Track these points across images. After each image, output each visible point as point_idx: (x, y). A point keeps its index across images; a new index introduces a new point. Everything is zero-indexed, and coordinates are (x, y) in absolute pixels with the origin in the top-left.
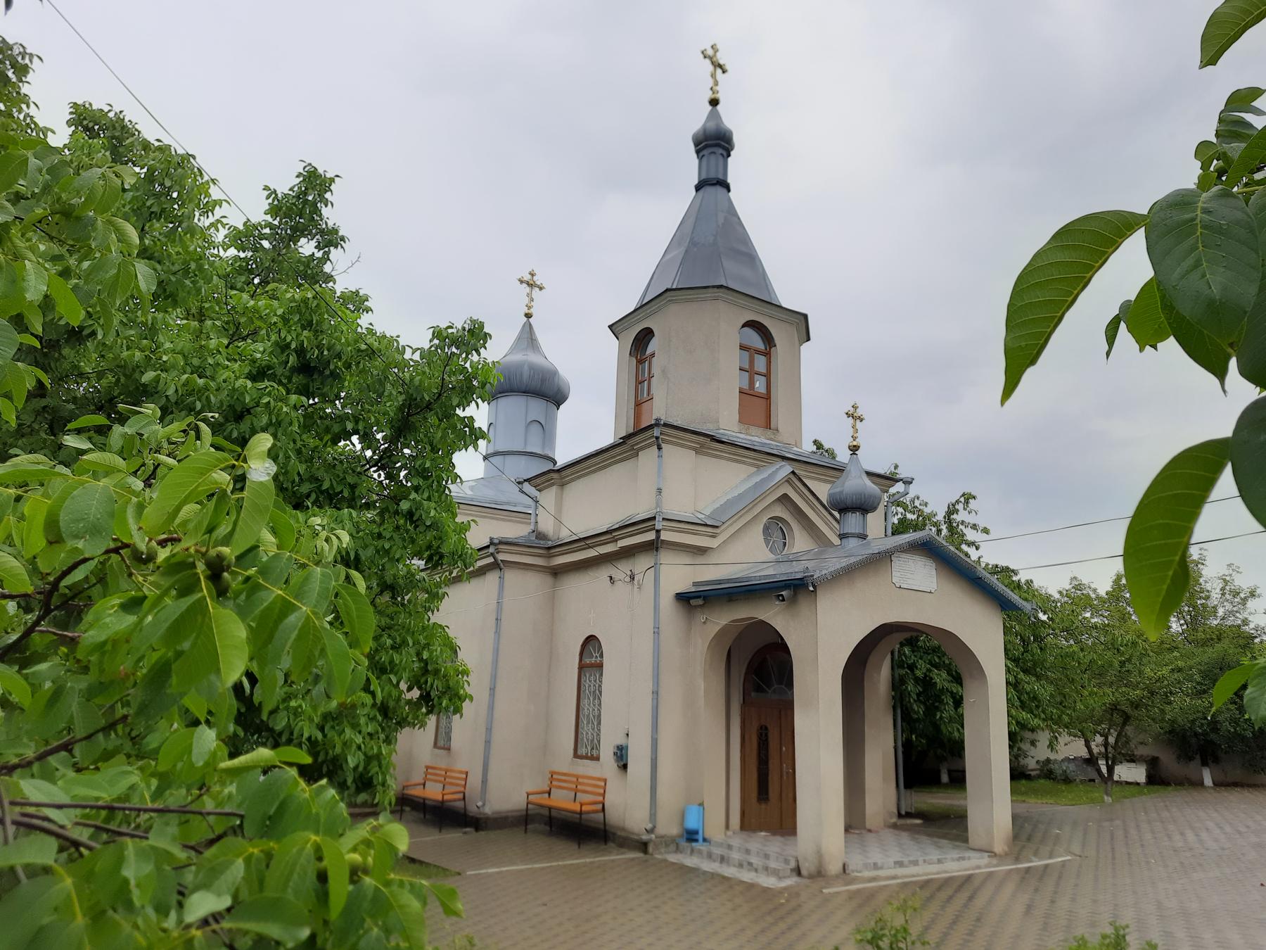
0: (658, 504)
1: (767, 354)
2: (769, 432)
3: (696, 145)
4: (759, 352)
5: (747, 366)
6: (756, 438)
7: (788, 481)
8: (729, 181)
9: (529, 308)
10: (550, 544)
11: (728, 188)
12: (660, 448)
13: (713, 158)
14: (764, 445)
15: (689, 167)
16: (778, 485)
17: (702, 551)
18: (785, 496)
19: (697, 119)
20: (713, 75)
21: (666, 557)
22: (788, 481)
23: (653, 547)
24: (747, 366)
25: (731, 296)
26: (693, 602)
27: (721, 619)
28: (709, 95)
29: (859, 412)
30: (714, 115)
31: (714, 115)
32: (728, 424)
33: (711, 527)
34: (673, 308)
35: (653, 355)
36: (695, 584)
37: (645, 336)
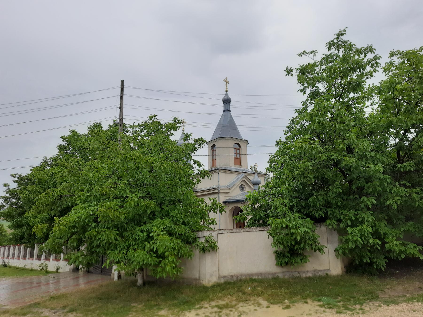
0: (219, 185)
1: (240, 149)
2: (240, 166)
3: (223, 102)
4: (238, 149)
5: (235, 152)
6: (238, 168)
7: (244, 177)
8: (231, 110)
9: (183, 128)
10: (196, 191)
11: (230, 111)
12: (218, 173)
13: (227, 105)
14: (239, 170)
15: (221, 107)
16: (243, 178)
17: (228, 193)
18: (244, 180)
19: (223, 97)
20: (226, 85)
21: (221, 195)
22: (244, 177)
23: (218, 193)
24: (235, 152)
25: (231, 139)
26: (226, 203)
27: (232, 206)
28: (225, 90)
29: (257, 165)
30: (227, 95)
31: (227, 95)
32: (232, 165)
33: (229, 188)
34: (220, 141)
35: (216, 150)
36: (226, 200)
37: (213, 146)
